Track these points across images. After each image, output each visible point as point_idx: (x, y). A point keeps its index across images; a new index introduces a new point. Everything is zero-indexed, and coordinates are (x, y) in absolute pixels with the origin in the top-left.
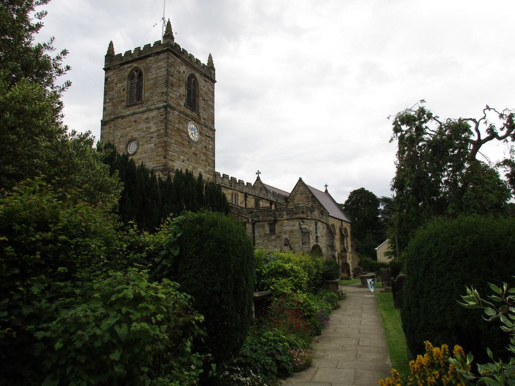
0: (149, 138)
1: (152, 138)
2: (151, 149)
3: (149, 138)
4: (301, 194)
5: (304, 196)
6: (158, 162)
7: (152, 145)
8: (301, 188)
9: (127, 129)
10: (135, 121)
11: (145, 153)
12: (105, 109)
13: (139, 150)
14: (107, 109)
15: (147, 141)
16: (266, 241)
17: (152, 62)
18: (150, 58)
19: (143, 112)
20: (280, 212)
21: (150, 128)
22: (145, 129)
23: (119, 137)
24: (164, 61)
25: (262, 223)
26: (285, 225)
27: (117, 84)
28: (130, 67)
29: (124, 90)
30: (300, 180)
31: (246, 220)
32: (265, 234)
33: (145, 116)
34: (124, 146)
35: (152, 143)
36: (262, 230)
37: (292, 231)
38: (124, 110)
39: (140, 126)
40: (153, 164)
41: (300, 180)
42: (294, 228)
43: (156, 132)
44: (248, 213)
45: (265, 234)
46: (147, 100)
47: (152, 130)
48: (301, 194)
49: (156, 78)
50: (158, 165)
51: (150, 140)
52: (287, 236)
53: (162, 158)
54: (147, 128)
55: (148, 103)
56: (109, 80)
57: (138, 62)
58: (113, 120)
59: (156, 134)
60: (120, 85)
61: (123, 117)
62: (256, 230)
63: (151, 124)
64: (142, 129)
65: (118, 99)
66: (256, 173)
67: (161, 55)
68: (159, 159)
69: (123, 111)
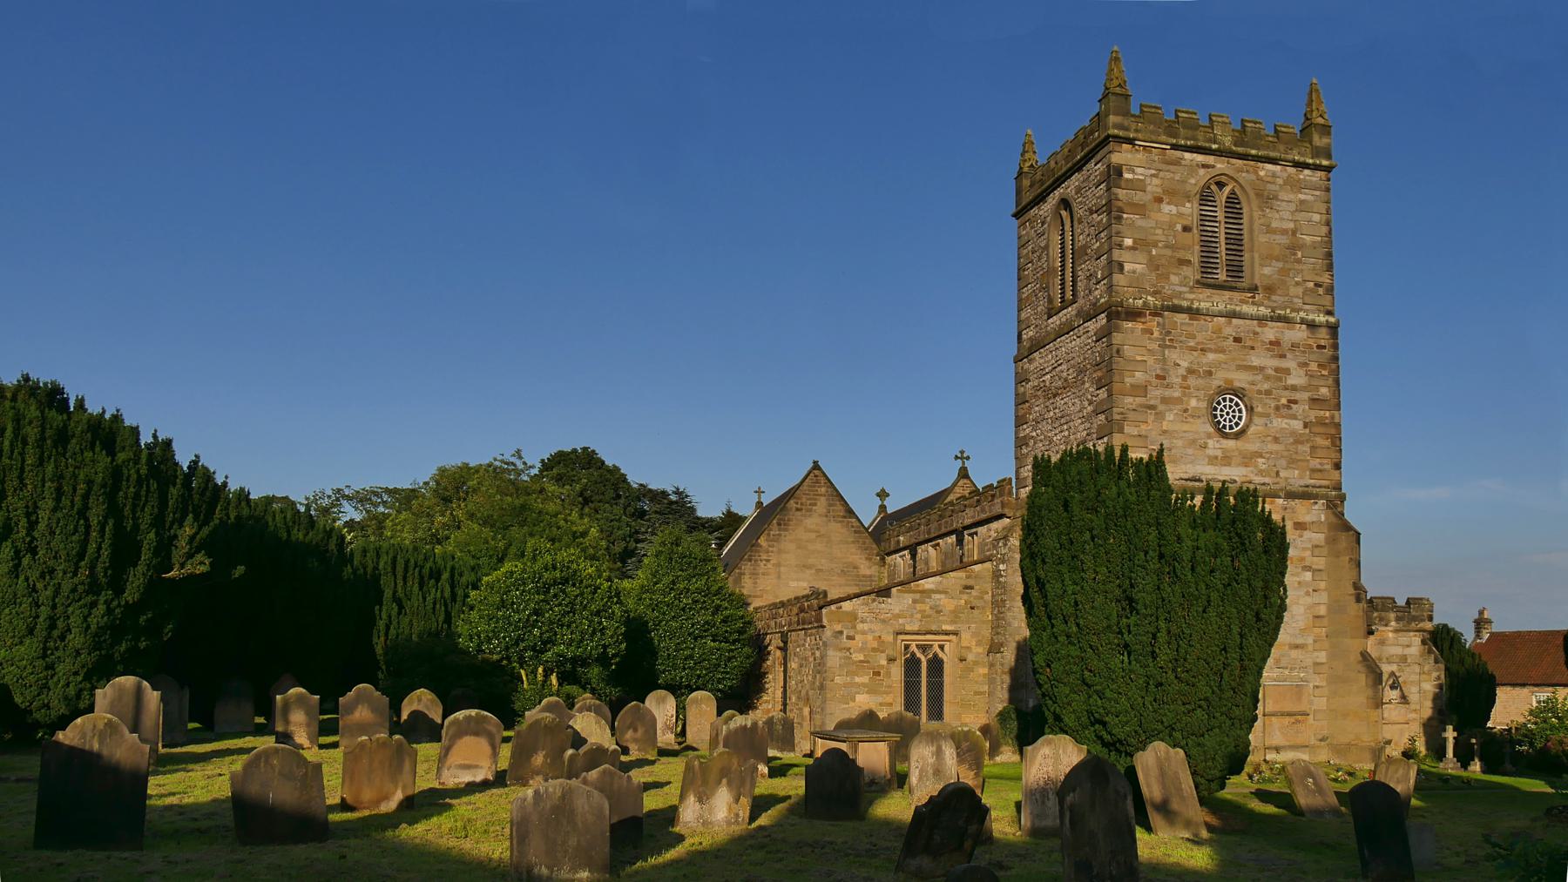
1: (1295, 402)
2: (1293, 433)
3: (1284, 401)
6: (1317, 475)
7: (1297, 425)
9: (1211, 356)
10: (1237, 340)
11: (1276, 440)
13: (1252, 429)
15: (1277, 408)
17: (1280, 181)
19: (1261, 320)
20: (1383, 614)
21: (1287, 371)
23: (1182, 371)
24: (1318, 193)
26: (1390, 642)
27: (1159, 200)
28: (1205, 166)
29: (1186, 229)
33: (1270, 332)
35: (1294, 417)
37: (1404, 659)
38: (1191, 293)
39: (1256, 361)
40: (1301, 477)
42: (1407, 651)
43: (1304, 389)
46: (1270, 290)
47: (1291, 381)
49: (1294, 232)
51: (1289, 407)
52: (1394, 668)
54: (1277, 370)
55: (1273, 298)
59: (1305, 396)
60: (1174, 209)
61: (1193, 313)
63: (1290, 363)
64: (1262, 369)
65: (1168, 252)
66: (957, 457)
68: (1319, 467)
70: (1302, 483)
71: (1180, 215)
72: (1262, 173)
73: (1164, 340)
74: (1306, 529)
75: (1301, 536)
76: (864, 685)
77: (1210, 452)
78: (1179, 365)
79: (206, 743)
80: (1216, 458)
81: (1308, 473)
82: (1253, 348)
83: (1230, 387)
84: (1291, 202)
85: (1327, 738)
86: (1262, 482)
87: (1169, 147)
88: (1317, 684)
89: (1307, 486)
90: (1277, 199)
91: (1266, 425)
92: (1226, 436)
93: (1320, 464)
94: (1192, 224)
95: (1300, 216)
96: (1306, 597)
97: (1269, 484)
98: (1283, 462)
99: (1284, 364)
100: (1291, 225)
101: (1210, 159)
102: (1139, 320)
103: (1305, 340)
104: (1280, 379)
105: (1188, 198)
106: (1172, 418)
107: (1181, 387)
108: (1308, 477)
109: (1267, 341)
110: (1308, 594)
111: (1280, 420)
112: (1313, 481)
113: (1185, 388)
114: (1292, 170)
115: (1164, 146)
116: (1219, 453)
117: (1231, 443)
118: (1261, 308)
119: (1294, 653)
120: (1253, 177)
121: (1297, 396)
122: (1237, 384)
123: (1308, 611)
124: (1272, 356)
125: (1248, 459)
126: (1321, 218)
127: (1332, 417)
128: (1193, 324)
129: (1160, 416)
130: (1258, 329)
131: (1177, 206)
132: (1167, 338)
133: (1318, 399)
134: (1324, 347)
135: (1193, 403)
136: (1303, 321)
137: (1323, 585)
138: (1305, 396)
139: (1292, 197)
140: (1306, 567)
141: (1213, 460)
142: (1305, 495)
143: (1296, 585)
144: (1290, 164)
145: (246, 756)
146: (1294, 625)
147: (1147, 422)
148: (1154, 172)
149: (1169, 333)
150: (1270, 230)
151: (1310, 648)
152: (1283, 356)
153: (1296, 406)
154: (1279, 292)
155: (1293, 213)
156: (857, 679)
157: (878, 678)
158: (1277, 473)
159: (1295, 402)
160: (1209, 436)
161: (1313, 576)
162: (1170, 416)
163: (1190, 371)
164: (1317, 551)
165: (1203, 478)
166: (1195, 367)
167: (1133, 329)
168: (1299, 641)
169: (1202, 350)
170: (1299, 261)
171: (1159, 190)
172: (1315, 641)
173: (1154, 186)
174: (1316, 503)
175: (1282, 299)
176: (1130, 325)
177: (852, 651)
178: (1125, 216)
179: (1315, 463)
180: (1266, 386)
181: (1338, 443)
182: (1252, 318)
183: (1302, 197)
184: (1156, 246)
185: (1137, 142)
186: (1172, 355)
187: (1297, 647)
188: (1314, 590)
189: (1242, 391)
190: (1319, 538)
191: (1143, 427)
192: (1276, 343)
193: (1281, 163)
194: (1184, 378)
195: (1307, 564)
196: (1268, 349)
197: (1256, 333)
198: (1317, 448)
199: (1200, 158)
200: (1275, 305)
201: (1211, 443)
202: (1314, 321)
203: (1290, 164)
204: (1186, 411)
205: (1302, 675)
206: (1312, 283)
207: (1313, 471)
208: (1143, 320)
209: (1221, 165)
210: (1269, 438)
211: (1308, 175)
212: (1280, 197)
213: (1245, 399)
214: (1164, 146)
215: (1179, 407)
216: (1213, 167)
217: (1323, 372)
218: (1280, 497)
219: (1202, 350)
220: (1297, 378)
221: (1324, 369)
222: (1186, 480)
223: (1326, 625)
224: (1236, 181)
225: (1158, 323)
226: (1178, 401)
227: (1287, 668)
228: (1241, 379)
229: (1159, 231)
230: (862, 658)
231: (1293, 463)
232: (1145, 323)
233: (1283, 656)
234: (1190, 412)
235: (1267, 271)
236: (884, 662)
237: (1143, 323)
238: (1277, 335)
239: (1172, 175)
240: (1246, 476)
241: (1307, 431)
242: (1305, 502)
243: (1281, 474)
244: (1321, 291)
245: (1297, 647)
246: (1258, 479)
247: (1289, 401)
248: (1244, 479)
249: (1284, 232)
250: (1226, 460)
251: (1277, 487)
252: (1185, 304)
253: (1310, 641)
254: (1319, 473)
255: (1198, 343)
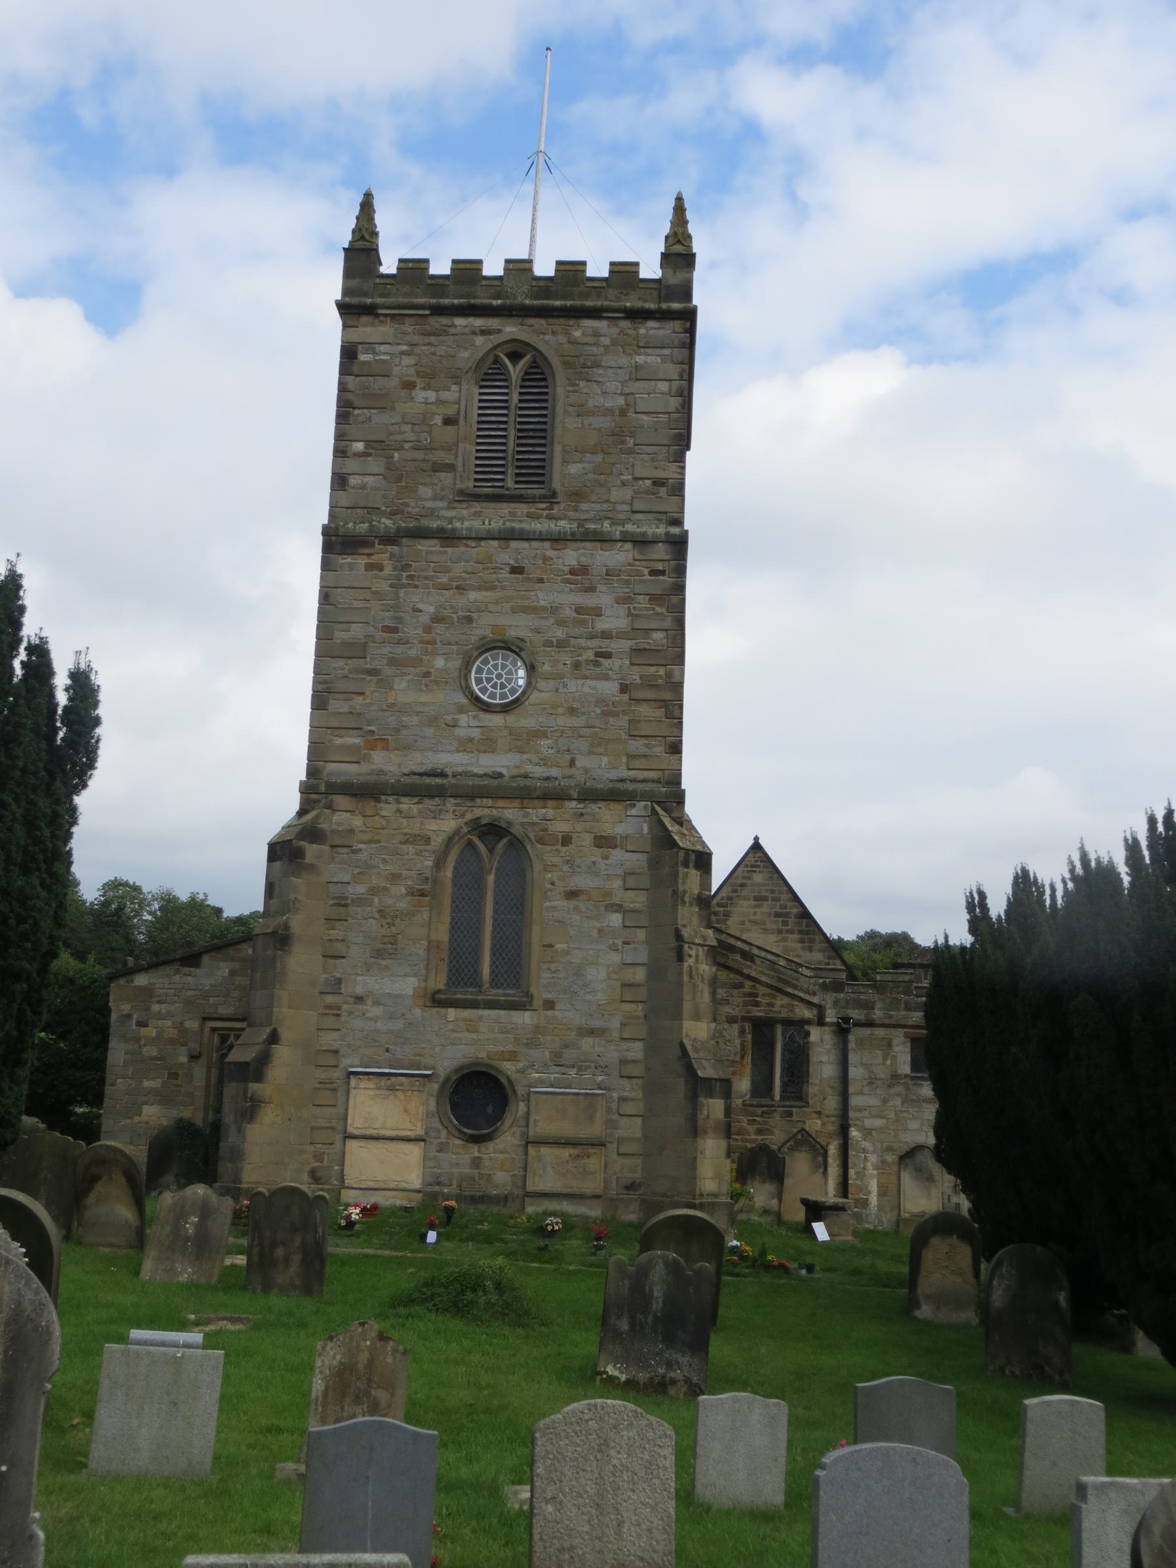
0: (590, 655)
1: (608, 656)
2: (600, 701)
3: (590, 655)
4: (756, 899)
5: (766, 907)
7: (609, 688)
8: (758, 878)
9: (473, 595)
10: (516, 570)
11: (572, 711)
12: (339, 481)
13: (534, 697)
14: (353, 481)
16: (898, 1102)
17: (606, 341)
18: (589, 323)
19: (558, 540)
21: (597, 612)
22: (569, 613)
23: (424, 619)
24: (667, 351)
25: (880, 1032)
27: (409, 386)
28: (485, 332)
30: (756, 847)
31: (807, 1013)
32: (895, 1078)
33: (571, 556)
34: (456, 663)
35: (605, 678)
36: (879, 1060)
38: (449, 508)
39: (543, 597)
41: (756, 847)
43: (622, 635)
44: (825, 987)
45: (895, 1078)
46: (577, 496)
47: (603, 625)
48: (756, 899)
49: (623, 412)
50: (641, 775)
51: (597, 664)
53: (659, 750)
54: (579, 610)
55: (584, 506)
56: (363, 357)
57: (532, 321)
58: (390, 539)
59: (626, 644)
60: (431, 395)
61: (448, 537)
62: (853, 1058)
63: (603, 598)
64: (554, 610)
67: (651, 324)
68: (643, 750)
69: (439, 504)
70: (613, 775)
71: (440, 402)
72: (577, 334)
73: (399, 578)
74: (615, 847)
75: (606, 858)
76: (150, 1091)
77: (460, 732)
78: (420, 611)
79: (126, 1154)
80: (471, 740)
81: (624, 760)
82: (541, 581)
83: (499, 638)
84: (620, 368)
85: (640, 1184)
86: (545, 775)
87: (427, 312)
88: (626, 1094)
89: (622, 780)
90: (599, 366)
91: (557, 690)
92: (486, 708)
93: (646, 746)
94: (458, 413)
95: (635, 387)
96: (612, 953)
97: (556, 779)
98: (583, 745)
99: (589, 600)
100: (621, 401)
101: (493, 323)
102: (360, 551)
103: (629, 564)
104: (583, 623)
105: (457, 379)
106: (404, 685)
107: (421, 642)
108: (624, 767)
109: (566, 569)
110: (614, 948)
111: (580, 682)
112: (632, 773)
113: (428, 643)
114: (625, 324)
115: (421, 312)
116: (476, 733)
117: (497, 720)
118: (562, 523)
119: (587, 1043)
120: (562, 339)
121: (614, 646)
122: (512, 633)
123: (614, 976)
124: (572, 591)
125: (523, 741)
126: (670, 386)
127: (669, 675)
128: (446, 553)
129: (385, 684)
130: (551, 553)
131: (437, 391)
132: (404, 574)
133: (645, 650)
134: (662, 573)
135: (440, 662)
136: (626, 538)
137: (641, 934)
138: (626, 644)
139: (623, 360)
140: (612, 905)
141: (466, 745)
142: (616, 795)
143: (595, 933)
144: (622, 315)
145: (145, 1170)
146: (588, 997)
147: (363, 694)
148: (405, 348)
149: (407, 567)
150: (583, 411)
151: (616, 1034)
152: (591, 589)
153: (610, 661)
154: (594, 498)
155: (623, 383)
156: (147, 1084)
157: (174, 1082)
158: (572, 763)
159: (608, 656)
160: (461, 710)
161: (624, 919)
162: (400, 684)
163: (437, 619)
164: (631, 882)
165: (448, 771)
166: (446, 613)
167: (351, 567)
168: (597, 1023)
169: (458, 588)
170: (630, 452)
171: (412, 371)
172: (623, 1025)
173: (405, 367)
174: (634, 805)
175: (598, 507)
176: (349, 560)
177: (143, 1042)
178: (357, 412)
179: (637, 746)
180: (560, 633)
181: (676, 713)
182: (541, 538)
183: (640, 359)
184: (400, 449)
185: (381, 311)
186: (412, 597)
187: (591, 1032)
188: (625, 943)
189: (520, 644)
190: (637, 861)
191: (359, 700)
192: (583, 570)
193: (605, 315)
194: (427, 629)
195: (616, 901)
196: (568, 582)
197: (546, 559)
198: (639, 721)
199: (478, 322)
200: (585, 516)
201: (463, 719)
202: (644, 534)
203: (622, 315)
204: (427, 675)
205: (600, 1079)
206: (648, 483)
207: (631, 757)
208: (366, 551)
209: (511, 329)
210: (560, 710)
211: (652, 328)
212: (603, 364)
213: (522, 654)
214: (421, 312)
215: (418, 670)
216: (499, 331)
217: (659, 610)
218: (571, 799)
219: (458, 588)
220: (614, 619)
221: (660, 606)
222: (421, 775)
223: (644, 999)
224: (535, 349)
225: (392, 555)
226: (417, 662)
227: (573, 1066)
228: (518, 626)
229: (406, 428)
230: (155, 1054)
231: (599, 744)
232: (371, 555)
233: (566, 1046)
234: (433, 678)
235: (574, 469)
236: (183, 1059)
237: (369, 555)
238: (583, 559)
239: (432, 349)
240: (518, 767)
241: (625, 697)
242: (613, 805)
243: (578, 764)
244: (663, 491)
245: (591, 1032)
246: (538, 771)
247: (598, 654)
248: (515, 772)
249: (609, 412)
250: (488, 744)
251: (572, 782)
252: (435, 524)
253: (615, 1023)
254: (643, 760)
255: (451, 579)
